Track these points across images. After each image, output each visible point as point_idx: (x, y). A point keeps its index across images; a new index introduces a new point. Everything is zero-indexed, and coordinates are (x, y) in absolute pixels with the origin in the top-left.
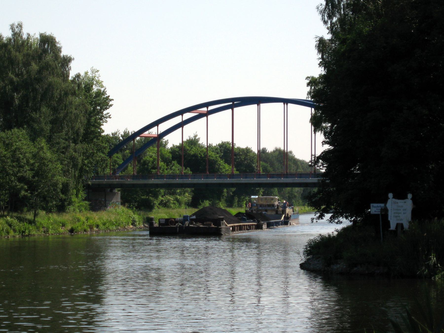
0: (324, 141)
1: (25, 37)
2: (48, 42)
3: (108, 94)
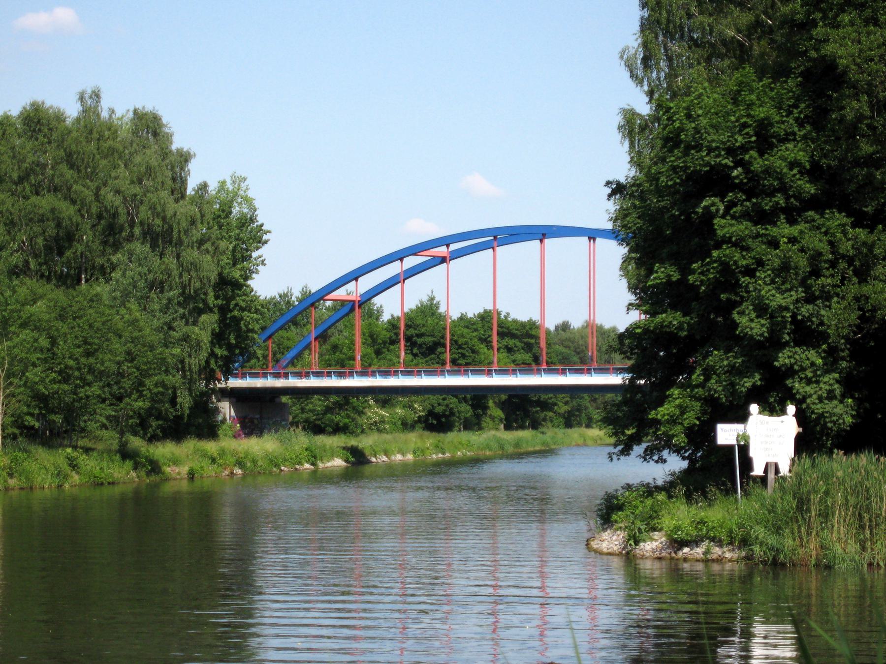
0: (630, 304)
1: (105, 114)
2: (149, 126)
3: (260, 219)
